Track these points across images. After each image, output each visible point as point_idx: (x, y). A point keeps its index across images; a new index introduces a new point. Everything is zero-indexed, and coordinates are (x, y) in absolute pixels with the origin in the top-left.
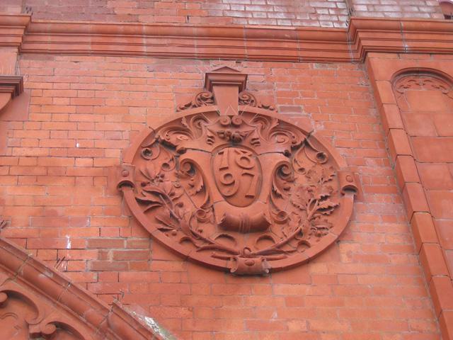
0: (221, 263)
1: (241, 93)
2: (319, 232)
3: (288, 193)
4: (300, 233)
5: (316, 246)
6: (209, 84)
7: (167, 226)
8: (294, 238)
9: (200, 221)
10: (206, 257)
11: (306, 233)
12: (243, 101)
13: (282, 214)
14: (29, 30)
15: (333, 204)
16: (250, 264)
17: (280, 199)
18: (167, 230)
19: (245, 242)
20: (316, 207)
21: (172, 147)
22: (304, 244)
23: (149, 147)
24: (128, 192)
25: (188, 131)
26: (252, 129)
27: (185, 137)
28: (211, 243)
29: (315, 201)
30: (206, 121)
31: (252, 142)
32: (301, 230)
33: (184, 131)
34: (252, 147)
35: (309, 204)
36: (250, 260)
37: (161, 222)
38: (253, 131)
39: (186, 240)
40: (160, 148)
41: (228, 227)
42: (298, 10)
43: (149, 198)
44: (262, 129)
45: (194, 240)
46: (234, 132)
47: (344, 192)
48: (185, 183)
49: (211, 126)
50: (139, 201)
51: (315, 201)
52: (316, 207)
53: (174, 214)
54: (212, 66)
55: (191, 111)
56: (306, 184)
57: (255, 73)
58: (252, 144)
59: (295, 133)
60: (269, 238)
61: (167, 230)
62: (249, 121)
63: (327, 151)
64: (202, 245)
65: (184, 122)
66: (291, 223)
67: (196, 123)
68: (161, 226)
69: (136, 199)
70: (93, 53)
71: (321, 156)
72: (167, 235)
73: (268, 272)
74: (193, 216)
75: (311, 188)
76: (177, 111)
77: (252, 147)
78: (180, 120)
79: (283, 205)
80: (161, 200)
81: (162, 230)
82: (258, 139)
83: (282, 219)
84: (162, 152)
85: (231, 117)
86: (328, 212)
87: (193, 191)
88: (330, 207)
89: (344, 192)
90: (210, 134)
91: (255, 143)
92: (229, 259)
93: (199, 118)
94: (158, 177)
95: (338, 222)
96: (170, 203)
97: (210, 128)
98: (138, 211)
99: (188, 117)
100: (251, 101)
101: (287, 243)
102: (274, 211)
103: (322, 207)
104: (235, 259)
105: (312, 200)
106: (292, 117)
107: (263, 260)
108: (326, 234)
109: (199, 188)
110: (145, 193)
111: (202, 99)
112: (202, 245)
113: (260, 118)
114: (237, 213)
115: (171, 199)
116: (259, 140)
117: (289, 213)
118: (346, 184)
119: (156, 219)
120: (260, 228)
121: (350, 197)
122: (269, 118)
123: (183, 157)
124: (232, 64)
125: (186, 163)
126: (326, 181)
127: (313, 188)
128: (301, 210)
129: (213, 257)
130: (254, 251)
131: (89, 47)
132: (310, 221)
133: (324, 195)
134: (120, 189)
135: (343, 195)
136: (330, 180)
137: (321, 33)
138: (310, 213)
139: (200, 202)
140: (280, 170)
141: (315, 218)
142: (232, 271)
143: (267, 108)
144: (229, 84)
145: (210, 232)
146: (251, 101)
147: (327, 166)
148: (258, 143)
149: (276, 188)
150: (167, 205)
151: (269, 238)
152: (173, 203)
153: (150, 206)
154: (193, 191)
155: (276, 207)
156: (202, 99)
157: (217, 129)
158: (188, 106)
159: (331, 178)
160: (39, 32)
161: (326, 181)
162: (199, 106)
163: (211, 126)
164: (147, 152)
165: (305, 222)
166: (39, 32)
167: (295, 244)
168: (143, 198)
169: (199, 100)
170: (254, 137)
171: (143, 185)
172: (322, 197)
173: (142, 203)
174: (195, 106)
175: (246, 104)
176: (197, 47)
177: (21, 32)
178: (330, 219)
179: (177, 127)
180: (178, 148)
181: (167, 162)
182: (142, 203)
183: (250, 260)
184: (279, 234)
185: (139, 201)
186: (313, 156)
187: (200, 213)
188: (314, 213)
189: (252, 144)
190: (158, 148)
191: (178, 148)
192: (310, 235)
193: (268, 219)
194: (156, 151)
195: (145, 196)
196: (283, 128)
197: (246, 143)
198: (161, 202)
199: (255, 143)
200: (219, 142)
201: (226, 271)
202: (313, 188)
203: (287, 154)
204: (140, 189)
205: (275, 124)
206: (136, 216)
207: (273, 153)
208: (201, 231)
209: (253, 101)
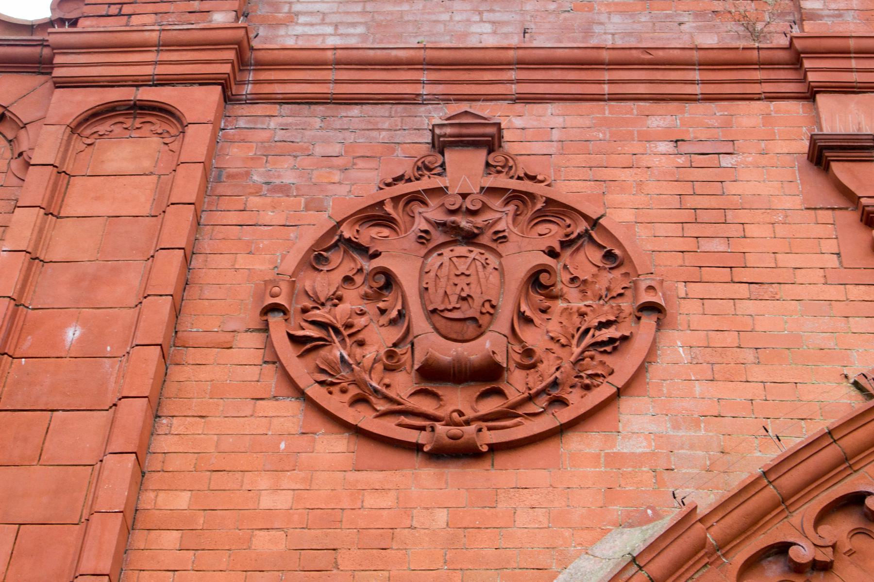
0: (412, 436)
1: (492, 155)
2: (587, 381)
3: (545, 316)
4: (555, 384)
5: (579, 403)
6: (440, 145)
7: (331, 376)
8: (543, 391)
9: (388, 369)
10: (389, 428)
11: (564, 384)
12: (495, 167)
13: (528, 352)
14: (245, 56)
15: (617, 335)
16: (454, 438)
17: (533, 328)
18: (332, 384)
19: (458, 400)
20: (588, 340)
21: (362, 250)
22: (562, 402)
23: (324, 250)
24: (275, 319)
25: (393, 220)
26: (498, 215)
27: (386, 232)
28: (399, 404)
29: (587, 331)
30: (425, 204)
31: (495, 238)
32: (556, 378)
33: (387, 221)
34: (494, 245)
35: (577, 336)
36: (454, 430)
37: (323, 371)
38: (500, 218)
39: (359, 400)
40: (344, 252)
41: (433, 374)
42: (596, 17)
43: (312, 332)
44: (516, 215)
45: (373, 399)
46: (464, 223)
47: (639, 314)
48: (371, 308)
49: (433, 212)
50: (293, 339)
51: (587, 331)
52: (588, 340)
53: (346, 357)
54: (437, 115)
55: (402, 188)
56: (578, 304)
57: (520, 125)
58: (496, 240)
59: (571, 218)
60: (500, 393)
61: (332, 384)
62: (496, 203)
63: (620, 246)
64: (382, 406)
65: (389, 208)
66: (541, 367)
67: (408, 208)
68: (323, 377)
69: (288, 334)
70: (703, 99)
71: (609, 255)
72: (330, 393)
73: (485, 449)
74: (375, 361)
75: (584, 309)
76: (381, 189)
77: (494, 245)
78: (381, 203)
79: (532, 337)
80: (330, 336)
81: (322, 383)
82: (504, 231)
83: (529, 360)
84: (345, 261)
85: (464, 196)
86: (609, 348)
87: (384, 320)
88: (612, 340)
89: (639, 314)
90: (425, 226)
91: (501, 238)
92: (422, 428)
93: (415, 198)
94: (332, 300)
95: (624, 365)
96: (343, 341)
97: (429, 216)
98: (287, 352)
99: (396, 200)
100: (506, 168)
101: (530, 399)
102: (518, 348)
103: (599, 339)
104: (433, 429)
105: (583, 328)
106: (565, 190)
107: (480, 430)
108: (598, 386)
109: (394, 314)
110: (304, 324)
111: (424, 168)
112: (382, 406)
113: (517, 197)
114: (447, 352)
115: (346, 333)
116: (506, 234)
117: (539, 352)
118: (646, 298)
119: (317, 366)
120: (487, 376)
121: (649, 321)
122: (532, 196)
123: (377, 263)
124: (465, 107)
125: (375, 275)
126: (613, 298)
127: (588, 310)
128: (563, 346)
129: (399, 425)
130: (470, 414)
131: (697, 89)
132: (575, 363)
133: (604, 320)
134: (265, 318)
135: (639, 318)
136: (620, 295)
137: (679, 51)
138: (577, 351)
139: (395, 334)
140: (536, 281)
141: (583, 359)
142: (425, 449)
143: (533, 178)
144: (474, 144)
145: (402, 385)
146: (506, 168)
147: (617, 273)
148: (505, 237)
149: (524, 308)
150: (338, 344)
151: (500, 393)
152: (347, 340)
153: (308, 346)
154: (384, 320)
155: (521, 341)
156: (424, 168)
157: (439, 216)
158: (398, 179)
159: (622, 291)
160: (263, 65)
161: (613, 298)
162: (418, 179)
163: (433, 212)
164: (320, 258)
165: (567, 366)
166: (263, 65)
167: (543, 401)
168: (300, 333)
169: (419, 169)
170: (499, 227)
171: (305, 311)
172: (600, 323)
173: (295, 340)
174: (409, 180)
175: (499, 172)
176: (425, 84)
177: (231, 55)
178: (609, 360)
179: (374, 216)
180: (371, 252)
181: (350, 274)
182: (295, 340)
183: (454, 430)
184: (517, 384)
185: (293, 339)
186: (596, 256)
187: (390, 354)
188: (583, 352)
189: (496, 240)
190: (342, 250)
191: (371, 252)
192: (572, 387)
193: (500, 358)
194: (335, 258)
195: (303, 329)
196: (555, 209)
197: (485, 239)
198: (329, 339)
199: (501, 238)
200: (438, 237)
201: (416, 448)
202: (588, 310)
203: (552, 253)
204: (296, 319)
205: (539, 206)
206: (284, 362)
207: (525, 252)
208: (388, 386)
209: (511, 167)
